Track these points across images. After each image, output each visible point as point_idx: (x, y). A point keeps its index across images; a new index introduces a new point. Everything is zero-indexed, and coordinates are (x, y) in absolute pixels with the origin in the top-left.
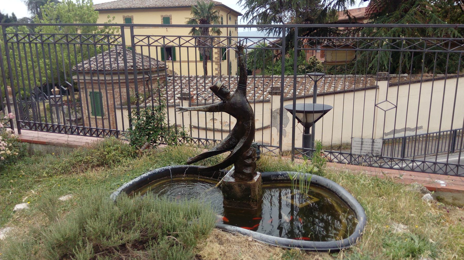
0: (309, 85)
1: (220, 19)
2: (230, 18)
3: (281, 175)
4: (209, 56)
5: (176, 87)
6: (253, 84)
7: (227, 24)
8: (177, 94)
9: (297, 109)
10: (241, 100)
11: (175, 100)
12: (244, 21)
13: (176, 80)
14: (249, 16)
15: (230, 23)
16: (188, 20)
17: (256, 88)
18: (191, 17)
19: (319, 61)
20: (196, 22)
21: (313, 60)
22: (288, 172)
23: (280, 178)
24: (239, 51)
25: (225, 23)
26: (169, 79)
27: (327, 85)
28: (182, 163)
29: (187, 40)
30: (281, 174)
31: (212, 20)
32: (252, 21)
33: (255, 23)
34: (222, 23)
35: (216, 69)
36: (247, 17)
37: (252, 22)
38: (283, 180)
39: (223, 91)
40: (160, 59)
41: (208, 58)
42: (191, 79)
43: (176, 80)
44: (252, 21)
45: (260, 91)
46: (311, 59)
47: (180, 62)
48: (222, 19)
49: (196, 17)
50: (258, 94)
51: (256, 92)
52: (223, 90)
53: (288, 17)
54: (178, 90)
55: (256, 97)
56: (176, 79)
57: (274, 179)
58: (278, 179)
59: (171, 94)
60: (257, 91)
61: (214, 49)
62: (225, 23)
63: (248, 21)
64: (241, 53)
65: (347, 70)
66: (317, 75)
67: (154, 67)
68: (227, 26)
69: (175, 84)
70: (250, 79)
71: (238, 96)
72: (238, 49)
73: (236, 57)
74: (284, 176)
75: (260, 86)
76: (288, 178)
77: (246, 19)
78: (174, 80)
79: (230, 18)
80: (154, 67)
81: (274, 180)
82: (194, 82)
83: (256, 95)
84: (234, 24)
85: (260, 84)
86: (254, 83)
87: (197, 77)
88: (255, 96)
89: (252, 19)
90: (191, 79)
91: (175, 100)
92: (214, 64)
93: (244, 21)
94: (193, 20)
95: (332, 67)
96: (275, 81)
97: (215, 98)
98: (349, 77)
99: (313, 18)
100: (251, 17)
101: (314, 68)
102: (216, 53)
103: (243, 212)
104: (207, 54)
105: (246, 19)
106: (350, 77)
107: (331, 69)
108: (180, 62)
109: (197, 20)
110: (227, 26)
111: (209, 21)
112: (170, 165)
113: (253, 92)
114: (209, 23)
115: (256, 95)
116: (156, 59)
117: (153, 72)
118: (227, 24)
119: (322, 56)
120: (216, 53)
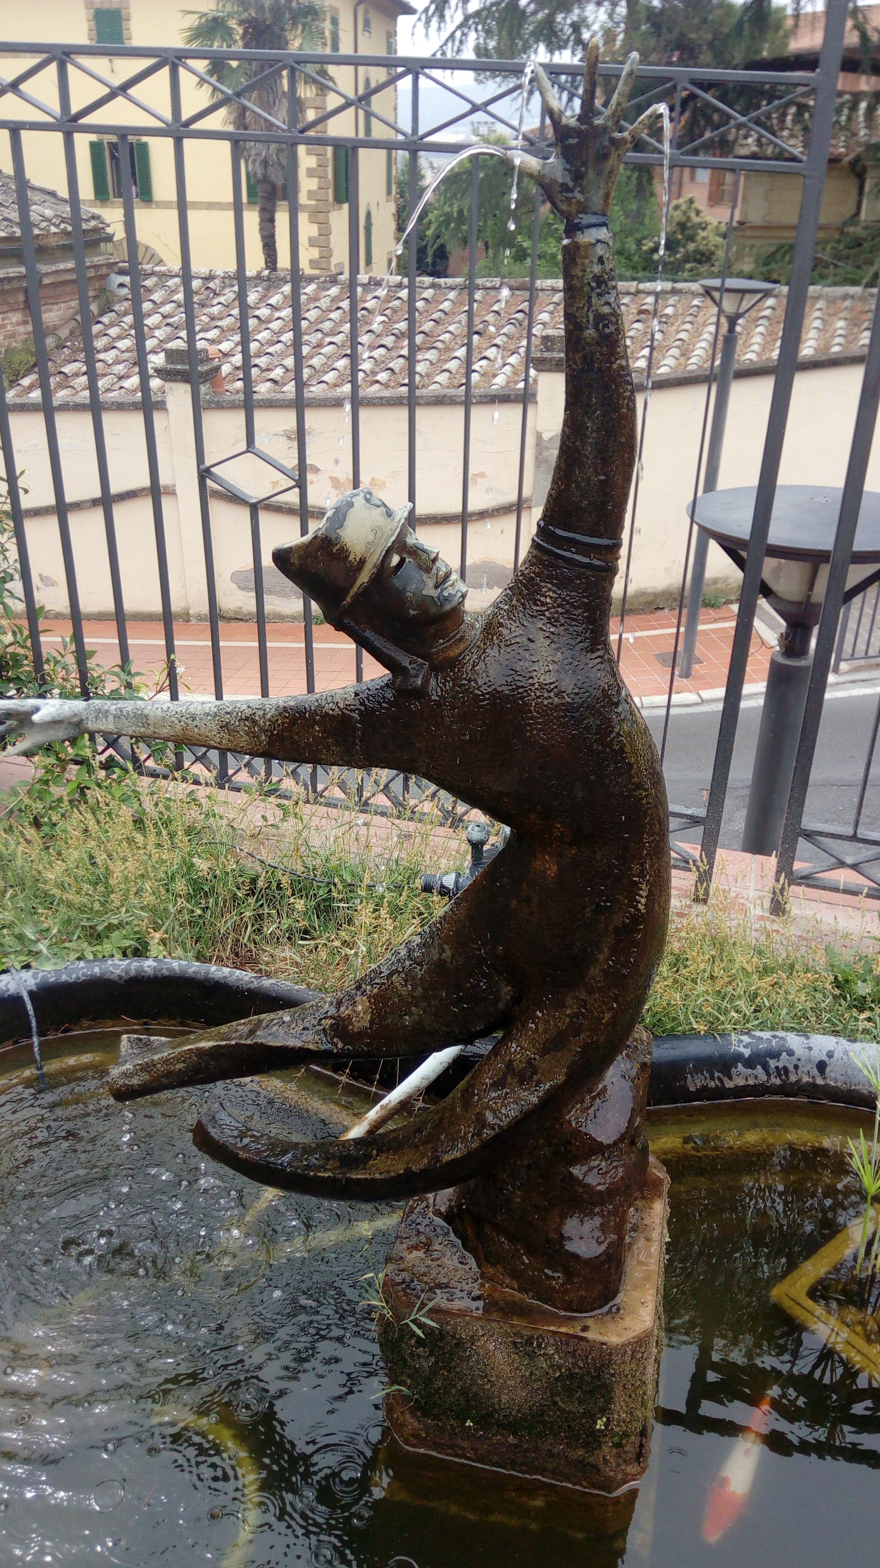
0: (688, 326)
1: (327, 26)
2: (367, 24)
3: (750, 1063)
4: (284, 187)
5: (149, 321)
6: (463, 317)
7: (356, 51)
8: (153, 352)
9: (777, 534)
10: (568, 684)
11: (145, 379)
12: (427, 35)
13: (149, 290)
14: (448, 13)
15: (369, 47)
16: (192, 21)
17: (476, 337)
18: (205, 10)
19: (708, 219)
20: (229, 32)
21: (685, 213)
22: (794, 1041)
23: (741, 1077)
24: (578, 177)
25: (346, 48)
26: (121, 285)
27: (761, 329)
28: (107, 947)
29: (117, 81)
30: (747, 1052)
31: (294, 25)
32: (458, 34)
33: (468, 54)
34: (335, 46)
35: (312, 243)
36: (442, 17)
37: (461, 42)
38: (758, 1090)
39: (399, 595)
40: (86, 189)
41: (279, 193)
42: (211, 285)
43: (149, 290)
44: (458, 34)
45: (494, 349)
46: (677, 208)
47: (182, 206)
48: (335, 22)
49: (229, 8)
50: (484, 363)
51: (475, 356)
52: (397, 582)
53: (596, 27)
54: (157, 333)
55: (475, 377)
56: (149, 283)
57: (705, 1088)
58: (729, 1084)
59: (128, 350)
60: (481, 350)
61: (301, 149)
62: (346, 48)
63: (445, 35)
64: (597, 201)
65: (836, 266)
66: (744, 292)
67: (53, 229)
68: (355, 61)
69: (146, 306)
70: (452, 295)
71: (543, 648)
72: (567, 154)
73: (389, 192)
74: (765, 1067)
75: (492, 329)
76: (793, 1078)
77: (434, 22)
78: (136, 287)
79: (367, 24)
80: (53, 229)
81: (703, 1093)
82: (222, 299)
83: (476, 367)
84: (384, 54)
85: (490, 318)
86: (470, 312)
87: (240, 276)
88: (469, 372)
89: (460, 26)
90: (211, 285)
91: (145, 379)
92: (303, 218)
93: (427, 35)
94: (215, 19)
95: (773, 249)
96: (551, 307)
97: (310, 377)
98: (845, 297)
99: (693, 36)
100: (459, 18)
101: (684, 246)
102: (311, 173)
103: (539, 1503)
104: (277, 178)
105: (434, 22)
106: (852, 297)
107: (769, 259)
108: (182, 206)
109: (233, 23)
110: (355, 61)
111: (283, 29)
112: (27, 967)
113: (461, 352)
114: (281, 43)
115: (476, 367)
116: (63, 192)
117: (43, 252)
118: (356, 51)
119: (715, 198)
120: (311, 173)
